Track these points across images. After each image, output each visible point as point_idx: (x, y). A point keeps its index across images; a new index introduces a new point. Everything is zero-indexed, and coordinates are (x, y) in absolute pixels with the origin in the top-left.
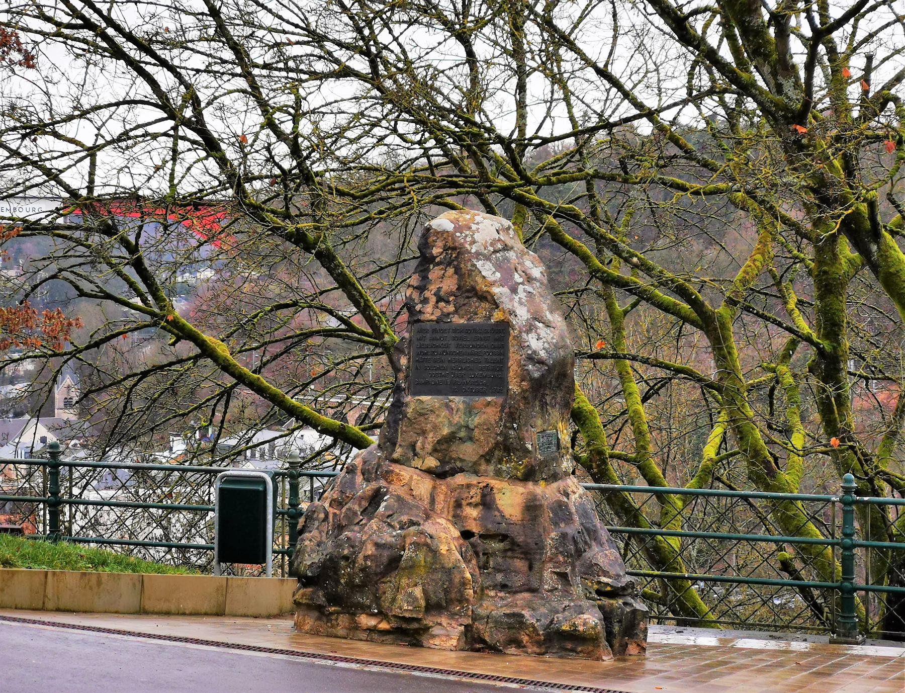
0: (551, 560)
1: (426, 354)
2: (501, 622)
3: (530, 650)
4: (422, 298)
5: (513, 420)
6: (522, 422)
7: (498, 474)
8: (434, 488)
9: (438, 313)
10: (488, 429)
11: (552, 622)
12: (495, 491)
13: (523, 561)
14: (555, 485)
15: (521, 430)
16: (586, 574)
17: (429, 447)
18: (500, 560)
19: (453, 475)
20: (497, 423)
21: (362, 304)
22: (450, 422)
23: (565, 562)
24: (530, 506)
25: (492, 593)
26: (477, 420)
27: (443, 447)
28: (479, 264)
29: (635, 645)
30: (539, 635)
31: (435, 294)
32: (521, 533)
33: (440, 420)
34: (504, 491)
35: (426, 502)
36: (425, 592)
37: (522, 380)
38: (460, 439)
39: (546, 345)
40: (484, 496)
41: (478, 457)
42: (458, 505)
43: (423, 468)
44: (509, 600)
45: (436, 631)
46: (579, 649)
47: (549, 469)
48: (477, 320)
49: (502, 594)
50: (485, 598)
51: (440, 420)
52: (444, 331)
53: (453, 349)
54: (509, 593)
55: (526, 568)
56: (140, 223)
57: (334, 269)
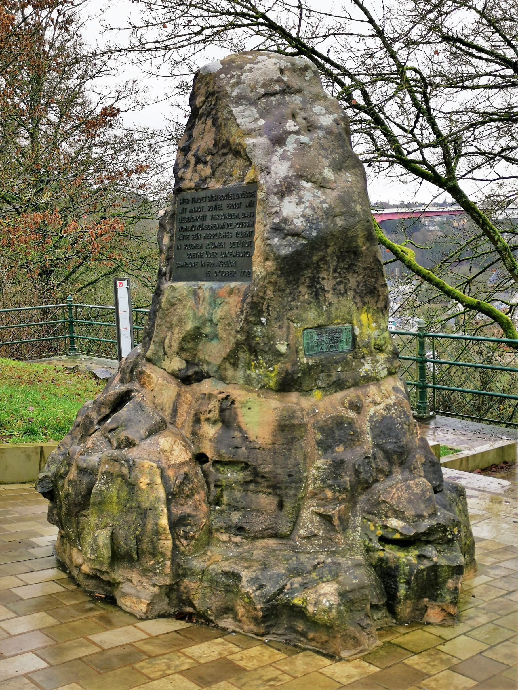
0: (314, 495)
1: (185, 230)
2: (217, 582)
3: (246, 628)
5: (260, 313)
6: (273, 314)
8: (179, 395)
9: (196, 179)
10: (229, 324)
11: (281, 591)
12: (237, 405)
13: (271, 497)
14: (339, 395)
15: (271, 326)
16: (369, 513)
17: (175, 345)
18: (238, 494)
19: (199, 381)
20: (238, 316)
21: (481, 222)
22: (195, 314)
23: (335, 499)
24: (286, 426)
25: (224, 537)
26: (219, 313)
27: (190, 345)
29: (437, 610)
30: (255, 609)
32: (269, 460)
34: (249, 405)
35: (168, 412)
36: (113, 537)
37: (267, 259)
38: (207, 336)
39: (308, 211)
40: (222, 411)
41: (221, 359)
42: (197, 421)
44: (246, 548)
45: (126, 588)
46: (311, 635)
47: (329, 376)
48: (232, 184)
49: (238, 539)
50: (214, 541)
51: (186, 311)
52: (201, 200)
53: (208, 222)
54: (246, 538)
55: (273, 507)
57: (460, 199)
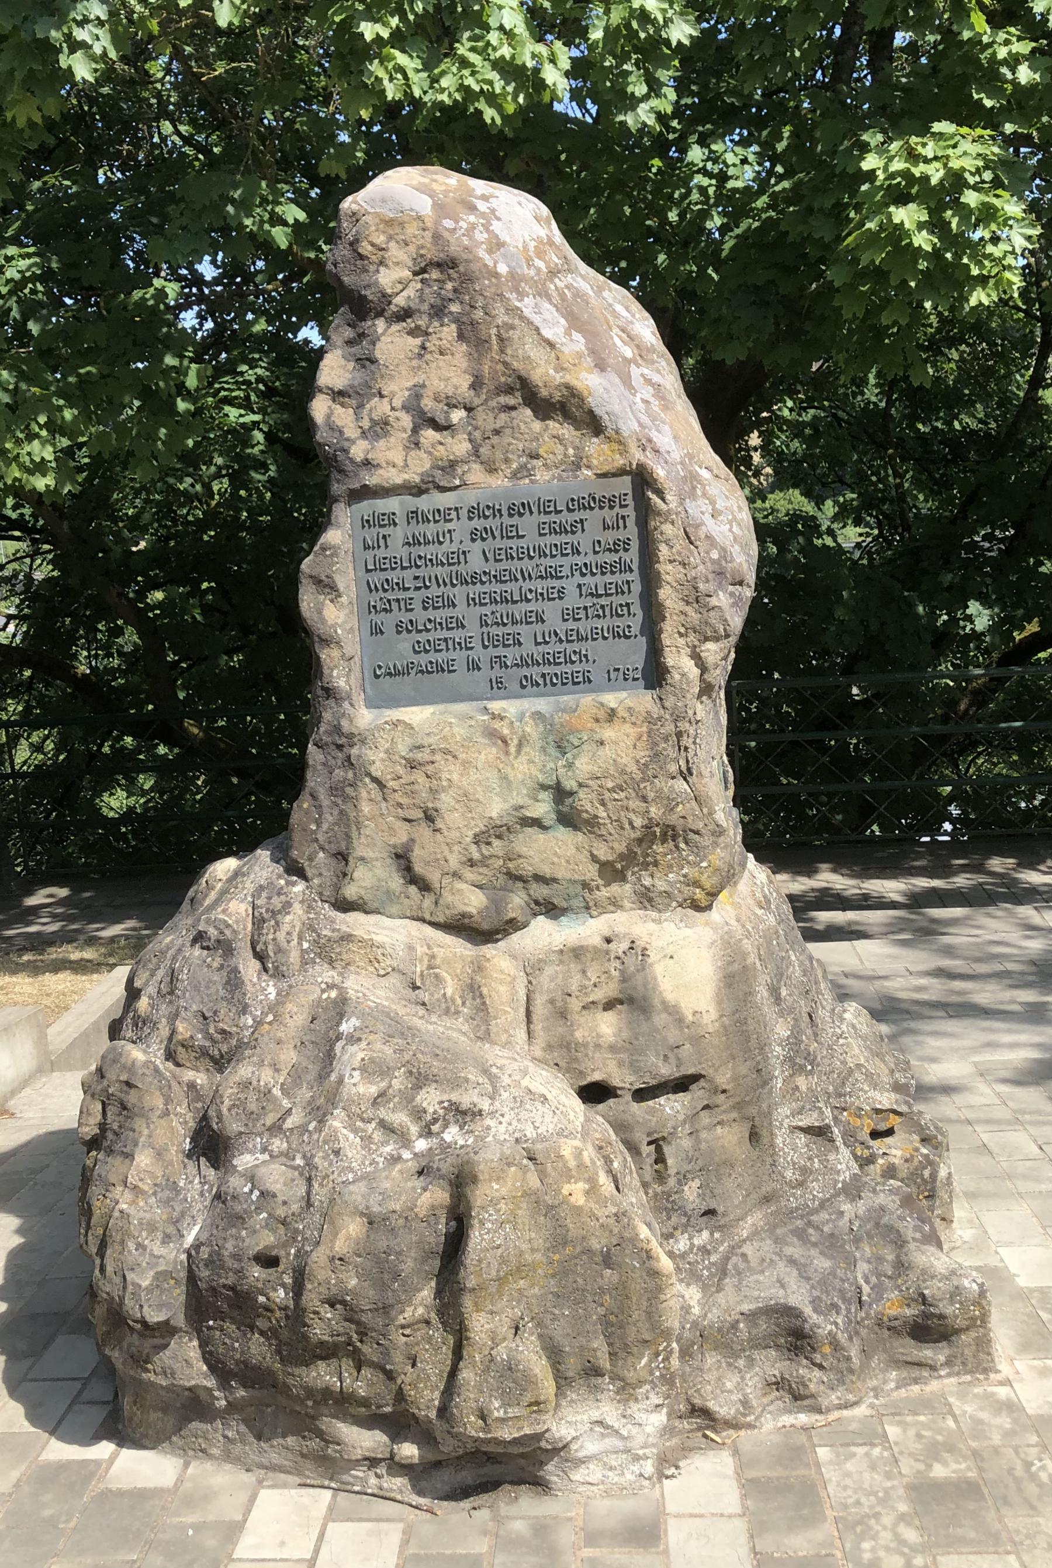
4: (366, 424)
7: (646, 899)
12: (653, 956)
28: (527, 305)
31: (405, 408)
33: (474, 776)
43: (441, 919)
53: (476, 563)
56: (579, 967)
